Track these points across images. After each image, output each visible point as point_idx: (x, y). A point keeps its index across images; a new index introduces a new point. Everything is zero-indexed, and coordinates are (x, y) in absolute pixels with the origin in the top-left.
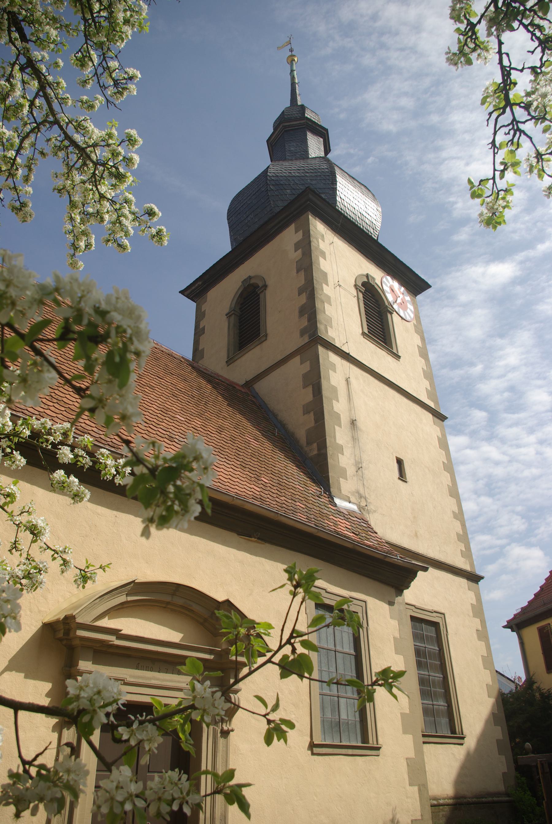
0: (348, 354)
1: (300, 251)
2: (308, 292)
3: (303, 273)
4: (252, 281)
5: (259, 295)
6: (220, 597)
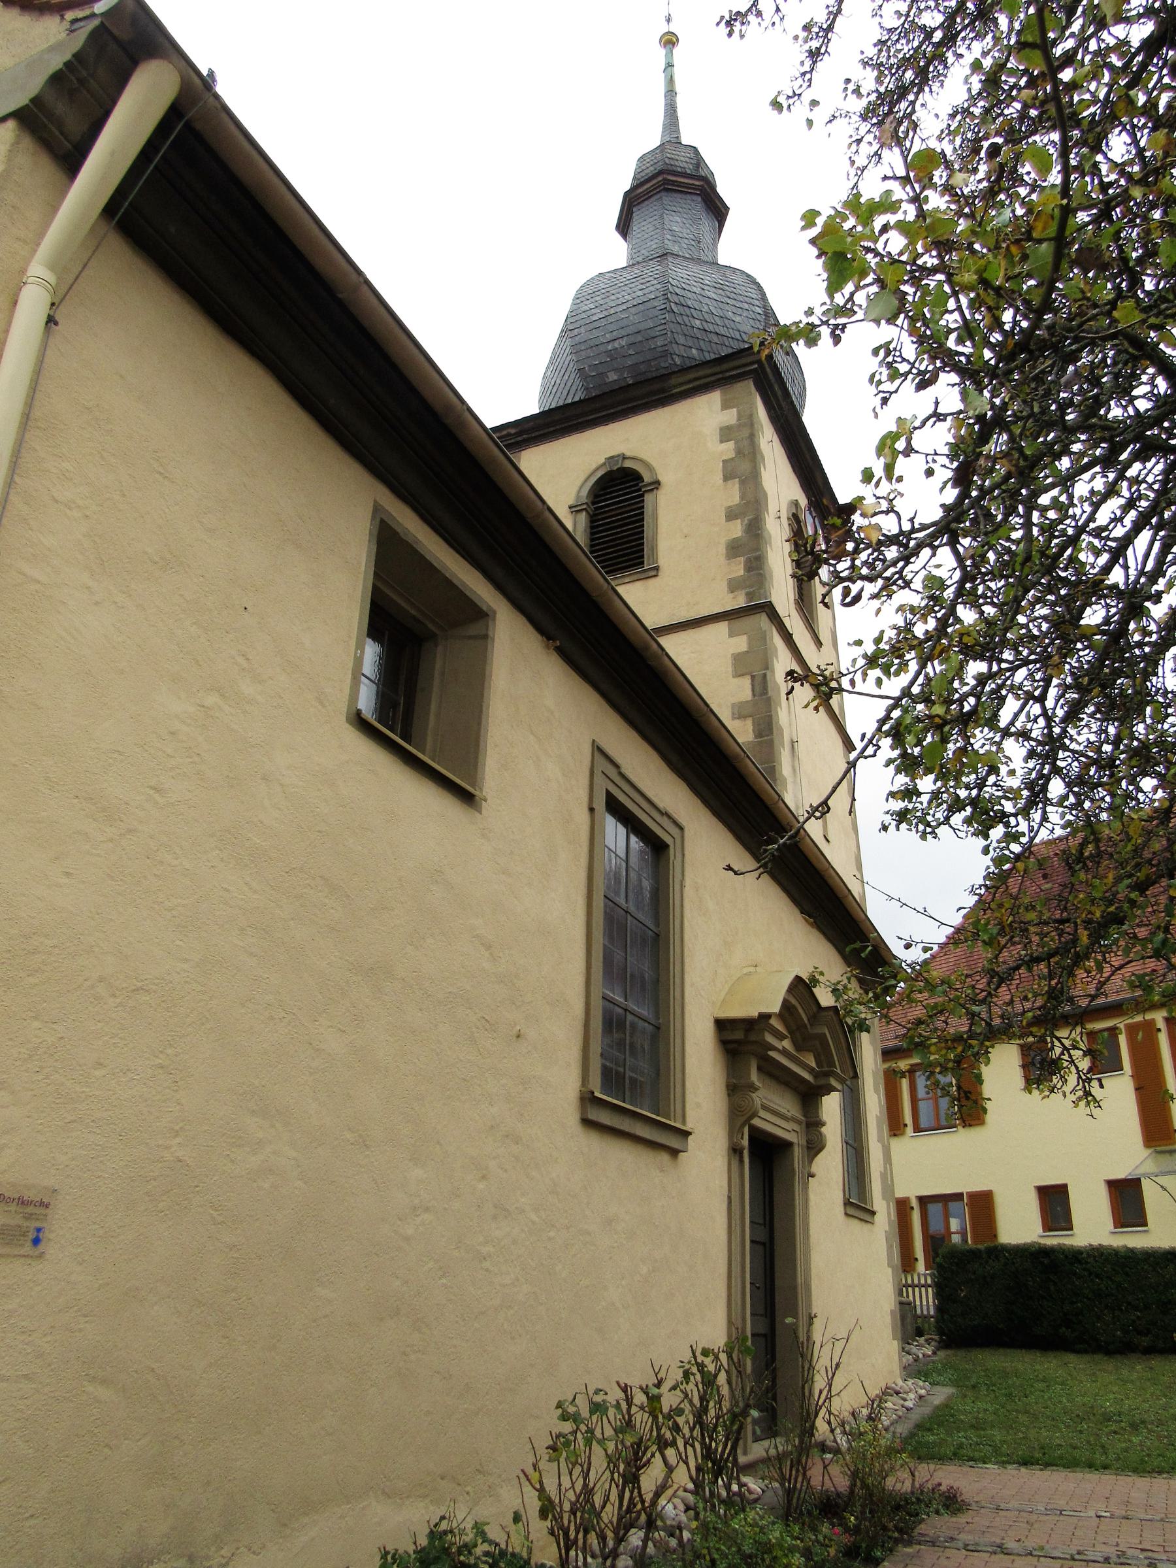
0: (791, 635)
1: (731, 445)
2: (746, 521)
3: (737, 486)
4: (628, 464)
5: (642, 495)
6: (754, 1014)
